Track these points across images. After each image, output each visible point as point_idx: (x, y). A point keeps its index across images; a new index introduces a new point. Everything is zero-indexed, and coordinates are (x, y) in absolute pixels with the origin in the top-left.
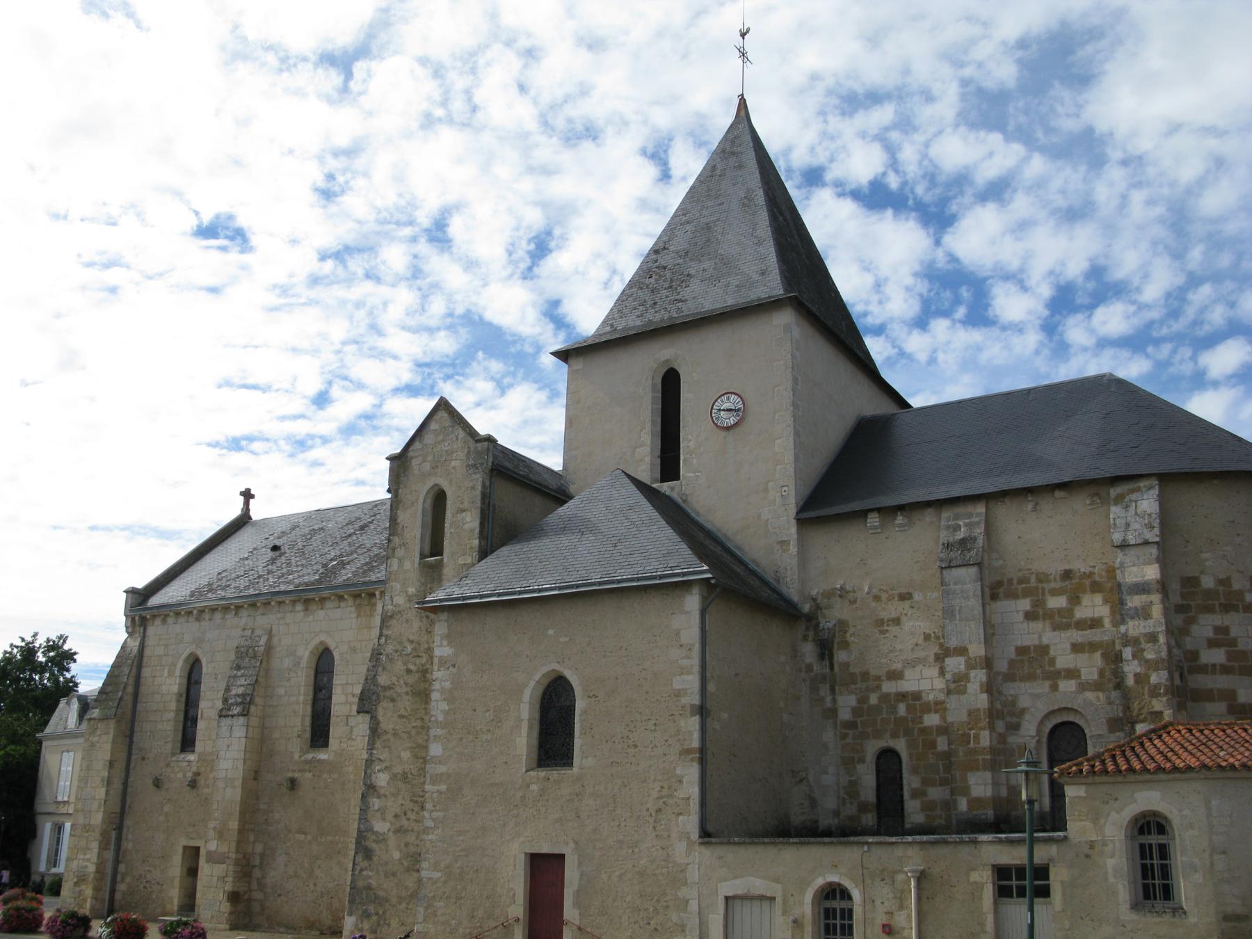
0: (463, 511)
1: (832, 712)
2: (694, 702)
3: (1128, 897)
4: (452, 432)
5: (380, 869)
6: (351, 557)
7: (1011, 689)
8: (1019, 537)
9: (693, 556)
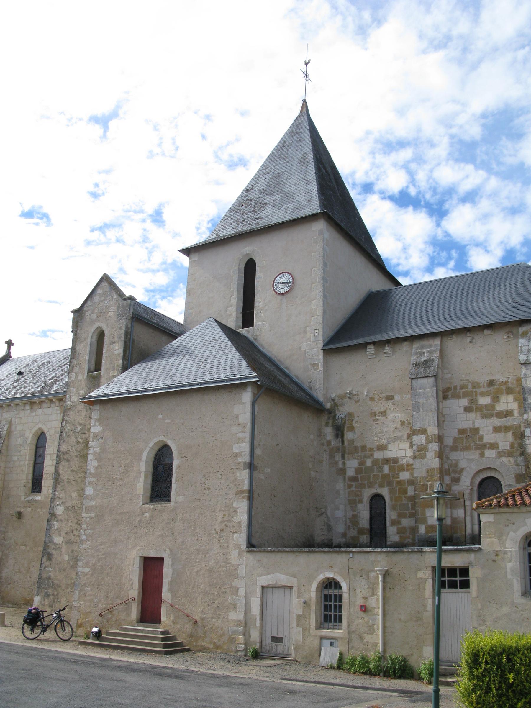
0: (114, 343)
1: (343, 471)
2: (245, 461)
3: (520, 588)
4: (110, 295)
5: (56, 566)
6: (61, 378)
7: (454, 456)
8: (462, 360)
9: (249, 368)
